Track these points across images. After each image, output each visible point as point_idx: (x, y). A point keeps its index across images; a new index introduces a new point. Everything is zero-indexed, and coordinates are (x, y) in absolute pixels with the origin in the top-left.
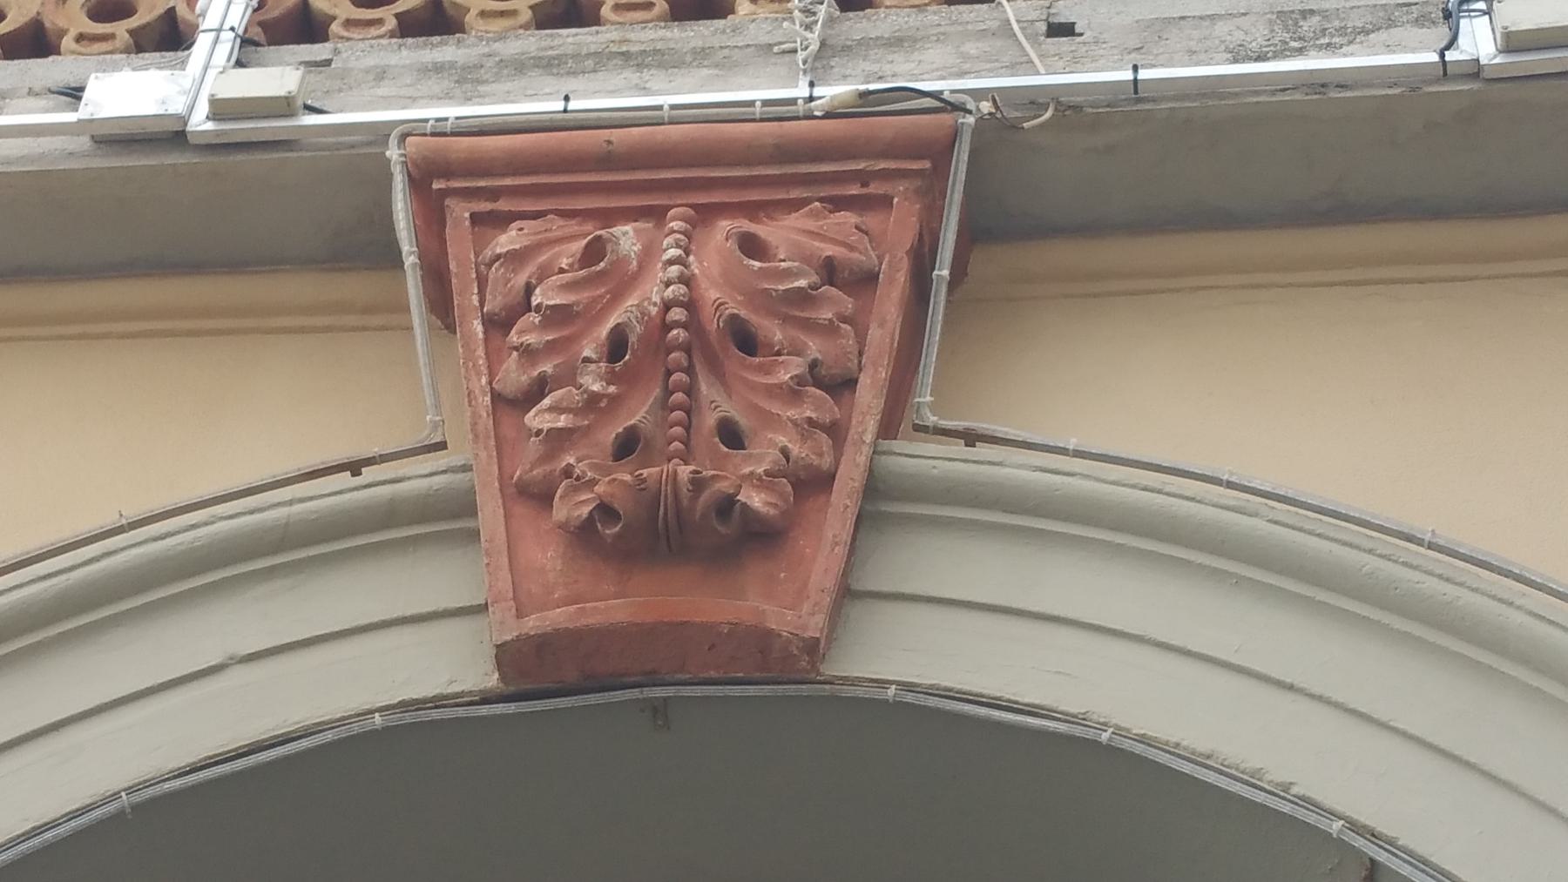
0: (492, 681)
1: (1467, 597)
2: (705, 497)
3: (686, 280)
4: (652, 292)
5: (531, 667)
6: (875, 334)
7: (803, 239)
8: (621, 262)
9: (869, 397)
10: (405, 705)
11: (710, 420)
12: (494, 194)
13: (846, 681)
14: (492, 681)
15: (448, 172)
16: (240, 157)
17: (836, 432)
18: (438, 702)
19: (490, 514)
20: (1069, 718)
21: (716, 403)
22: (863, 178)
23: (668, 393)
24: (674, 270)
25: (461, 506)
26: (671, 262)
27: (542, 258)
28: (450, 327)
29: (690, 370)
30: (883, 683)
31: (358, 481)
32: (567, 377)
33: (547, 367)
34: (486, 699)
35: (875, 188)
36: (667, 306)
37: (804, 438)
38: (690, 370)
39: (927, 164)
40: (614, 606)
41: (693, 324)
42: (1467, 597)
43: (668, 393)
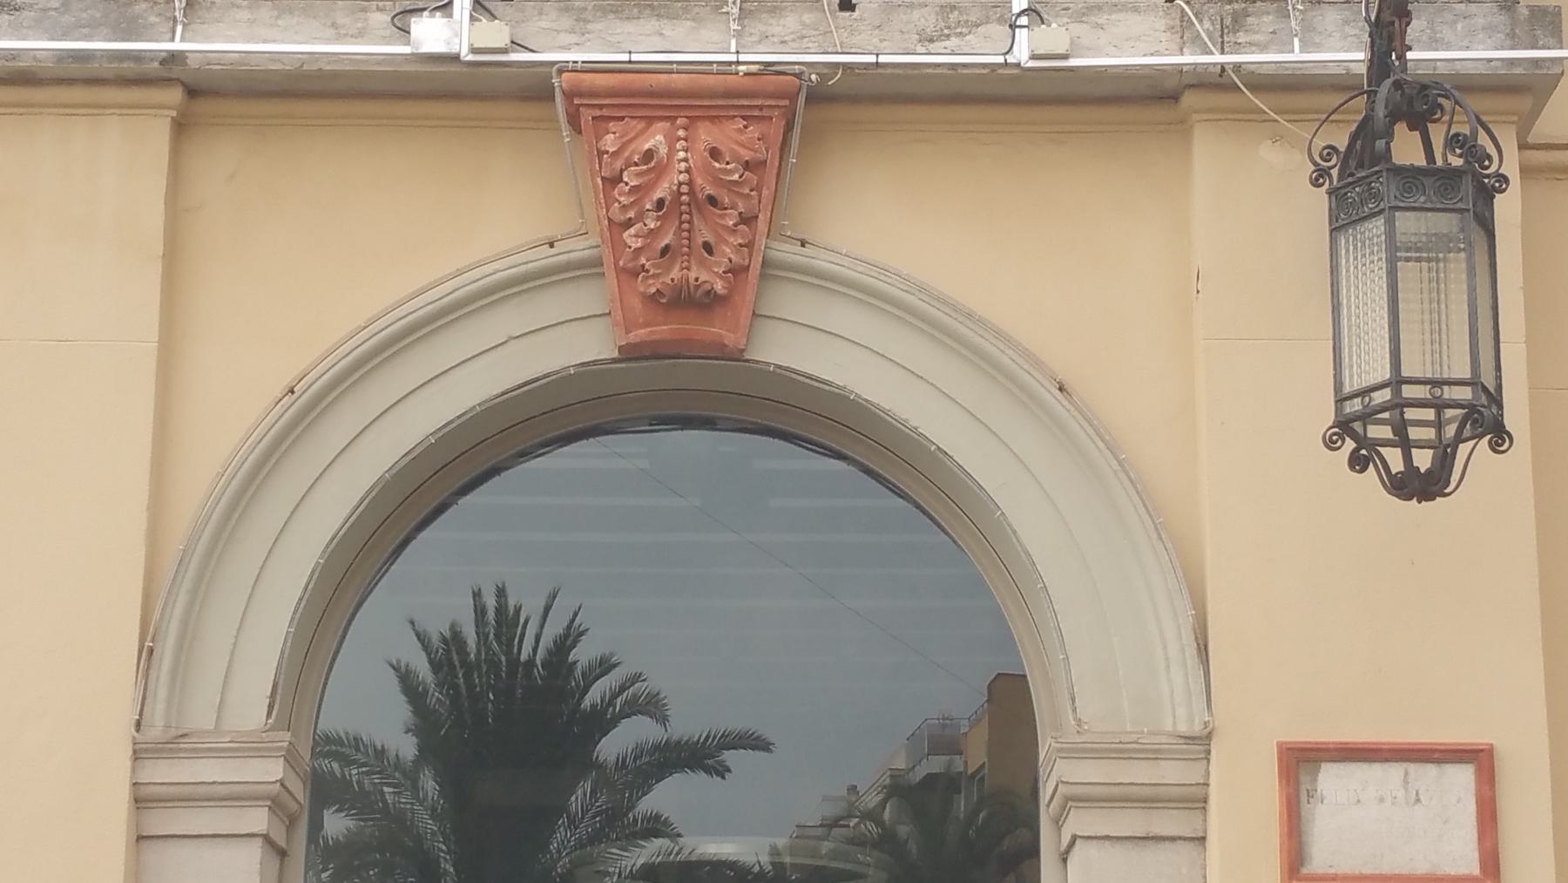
0: (616, 354)
1: (987, 345)
2: (700, 292)
3: (688, 171)
4: (676, 177)
5: (629, 353)
6: (765, 192)
7: (736, 147)
8: (659, 163)
9: (762, 225)
10: (583, 364)
11: (700, 241)
12: (601, 107)
13: (757, 362)
14: (616, 354)
15: (581, 95)
16: (485, 69)
17: (749, 245)
18: (594, 362)
19: (609, 269)
20: (838, 387)
21: (704, 234)
22: (760, 108)
23: (681, 223)
24: (683, 165)
25: (598, 262)
26: (680, 161)
27: (626, 154)
28: (580, 133)
29: (690, 213)
30: (768, 364)
31: (553, 251)
32: (640, 217)
33: (631, 214)
34: (614, 361)
35: (766, 113)
36: (680, 184)
37: (737, 252)
38: (690, 213)
39: (787, 102)
40: (664, 330)
41: (692, 193)
42: (987, 345)
43: (681, 223)
